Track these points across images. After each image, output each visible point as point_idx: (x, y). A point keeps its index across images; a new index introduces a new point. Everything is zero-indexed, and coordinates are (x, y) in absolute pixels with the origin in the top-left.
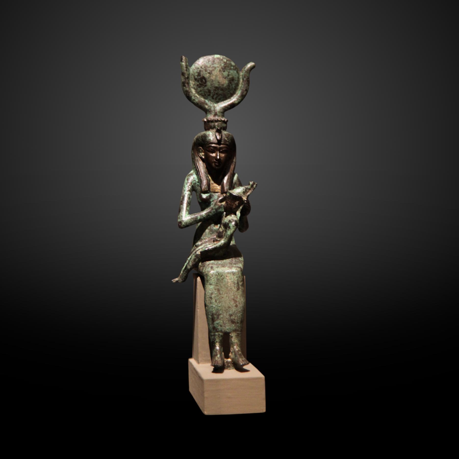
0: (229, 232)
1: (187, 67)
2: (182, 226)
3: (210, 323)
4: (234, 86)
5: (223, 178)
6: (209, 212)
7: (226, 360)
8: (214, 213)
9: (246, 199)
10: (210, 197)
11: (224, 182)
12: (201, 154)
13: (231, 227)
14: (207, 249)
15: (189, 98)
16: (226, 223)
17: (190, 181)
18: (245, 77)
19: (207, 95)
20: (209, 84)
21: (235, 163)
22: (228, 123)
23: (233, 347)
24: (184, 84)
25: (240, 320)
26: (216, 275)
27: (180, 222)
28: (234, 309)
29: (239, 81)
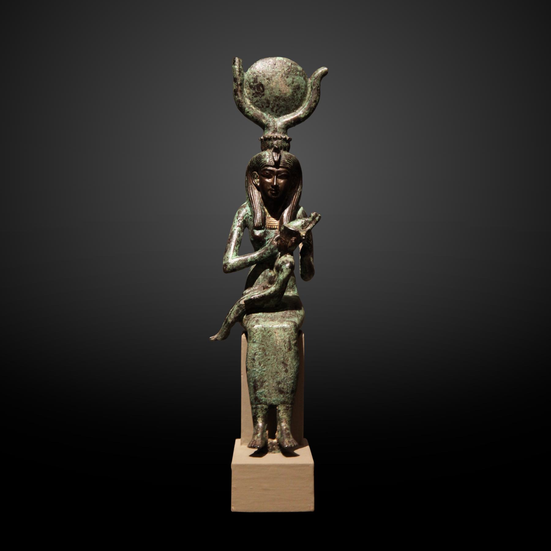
0: (282, 277)
1: (240, 72)
2: (227, 269)
3: (252, 392)
4: (299, 96)
5: (283, 211)
6: (262, 253)
7: (270, 440)
8: (268, 255)
9: (304, 235)
10: (265, 234)
11: (283, 216)
12: (256, 180)
13: (284, 270)
14: (252, 297)
15: (242, 109)
16: (278, 265)
17: (241, 215)
18: (314, 85)
19: (265, 107)
20: (267, 92)
21: (301, 192)
22: (291, 142)
23: (280, 424)
24: (235, 92)
25: (291, 389)
26: (262, 331)
27: (226, 265)
28: (283, 375)
29: (306, 89)
